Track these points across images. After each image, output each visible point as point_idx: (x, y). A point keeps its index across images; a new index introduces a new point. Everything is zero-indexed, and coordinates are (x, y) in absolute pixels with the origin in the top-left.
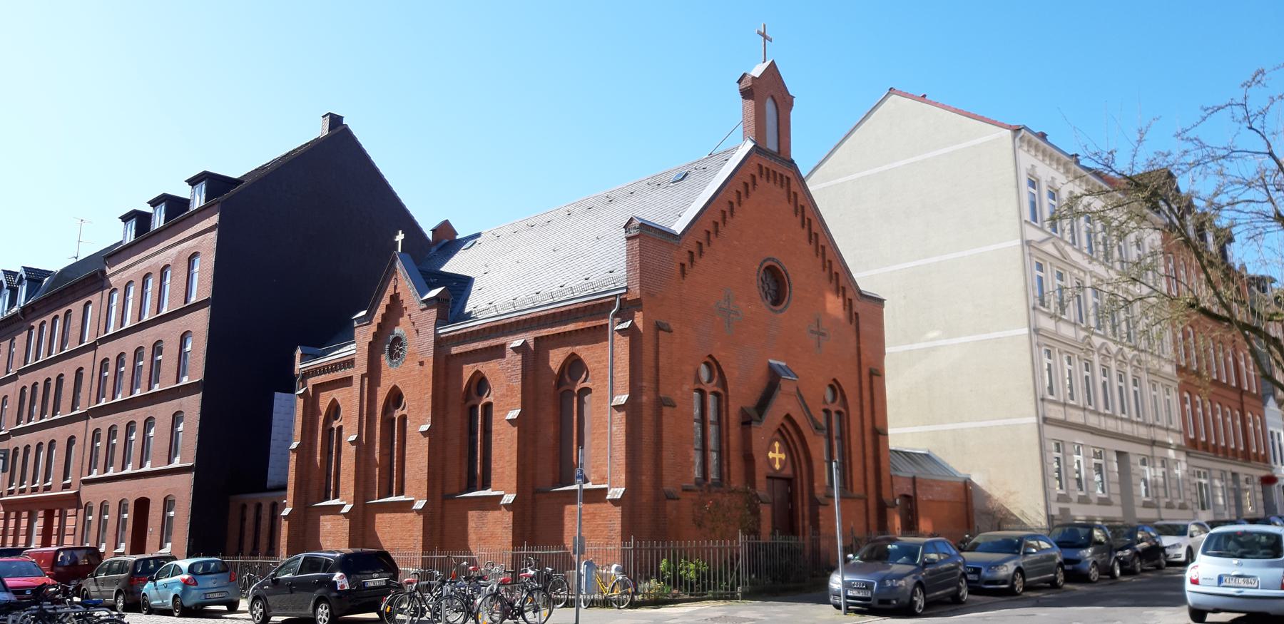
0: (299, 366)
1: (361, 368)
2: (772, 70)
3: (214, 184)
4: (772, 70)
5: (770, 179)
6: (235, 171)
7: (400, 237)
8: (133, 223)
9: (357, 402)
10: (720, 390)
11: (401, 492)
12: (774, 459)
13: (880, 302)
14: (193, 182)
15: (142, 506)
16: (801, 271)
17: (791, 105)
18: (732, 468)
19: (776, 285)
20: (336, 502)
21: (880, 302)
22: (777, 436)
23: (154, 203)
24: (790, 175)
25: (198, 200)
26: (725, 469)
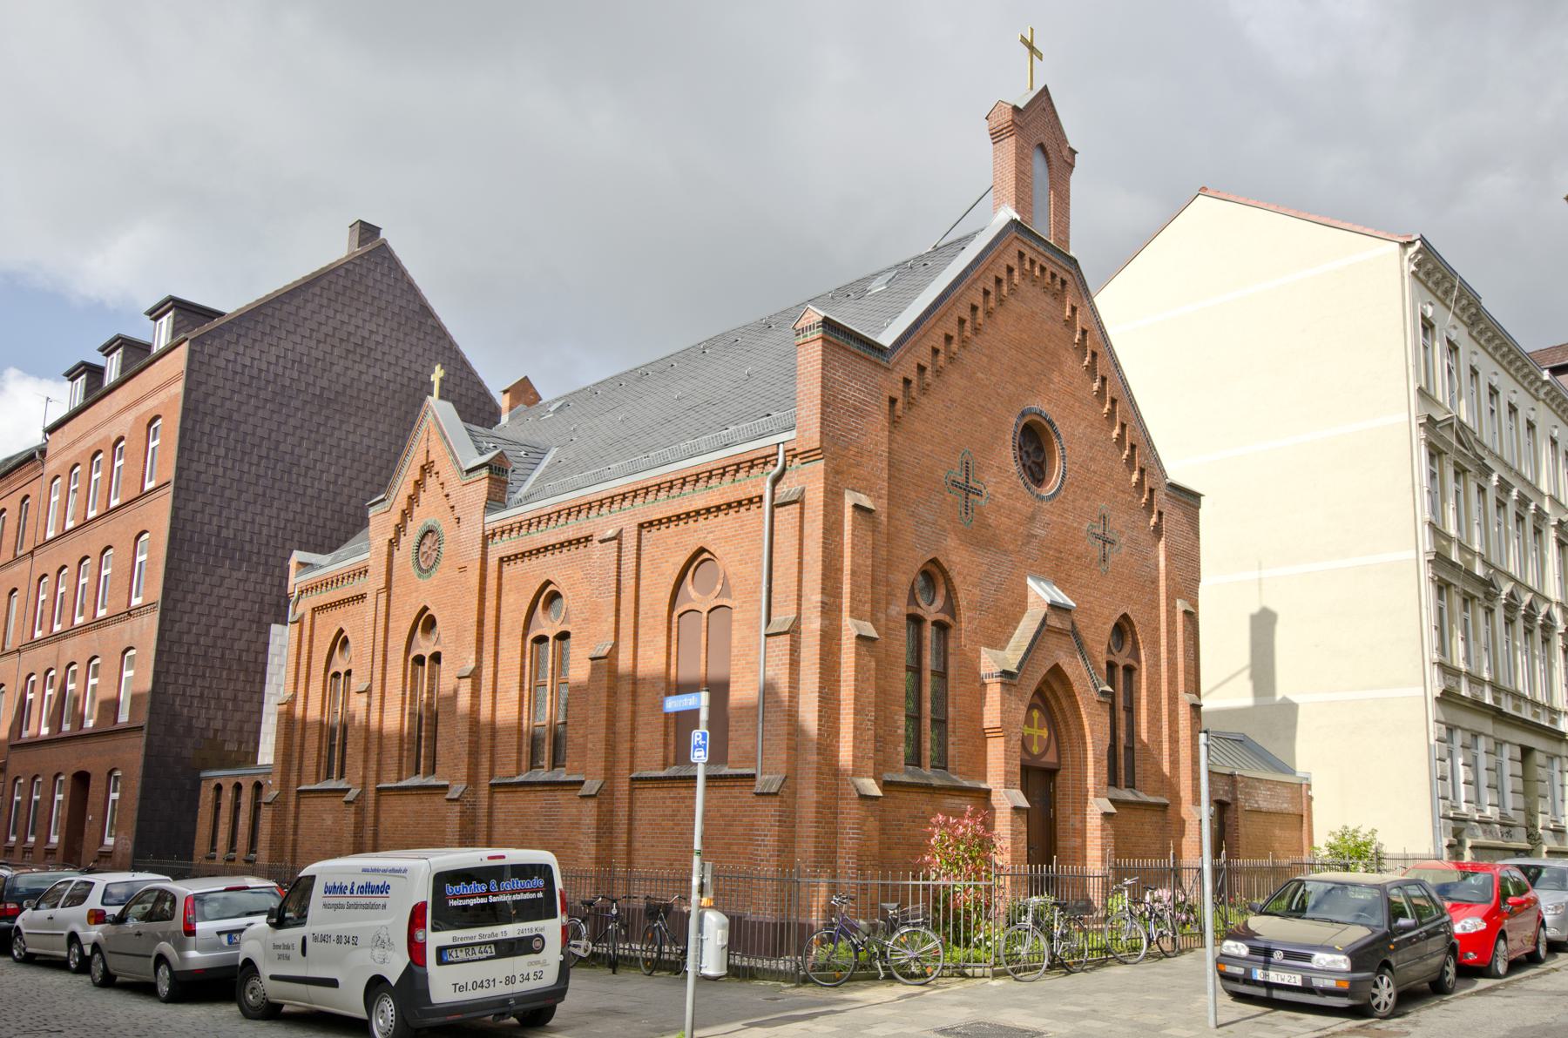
0: (295, 581)
1: (373, 583)
2: (1044, 97)
3: (187, 313)
4: (1044, 97)
5: (1032, 282)
6: (229, 300)
7: (437, 375)
8: (81, 381)
9: (370, 632)
10: (948, 619)
11: (432, 770)
12: (1040, 727)
13: (1195, 497)
14: (155, 314)
15: (556, 762)
16: (1075, 436)
17: (1071, 166)
18: (316, 744)
19: (1035, 442)
20: (342, 785)
21: (1195, 497)
22: (1038, 701)
23: (107, 350)
24: (1067, 277)
25: (160, 334)
26: (297, 739)
